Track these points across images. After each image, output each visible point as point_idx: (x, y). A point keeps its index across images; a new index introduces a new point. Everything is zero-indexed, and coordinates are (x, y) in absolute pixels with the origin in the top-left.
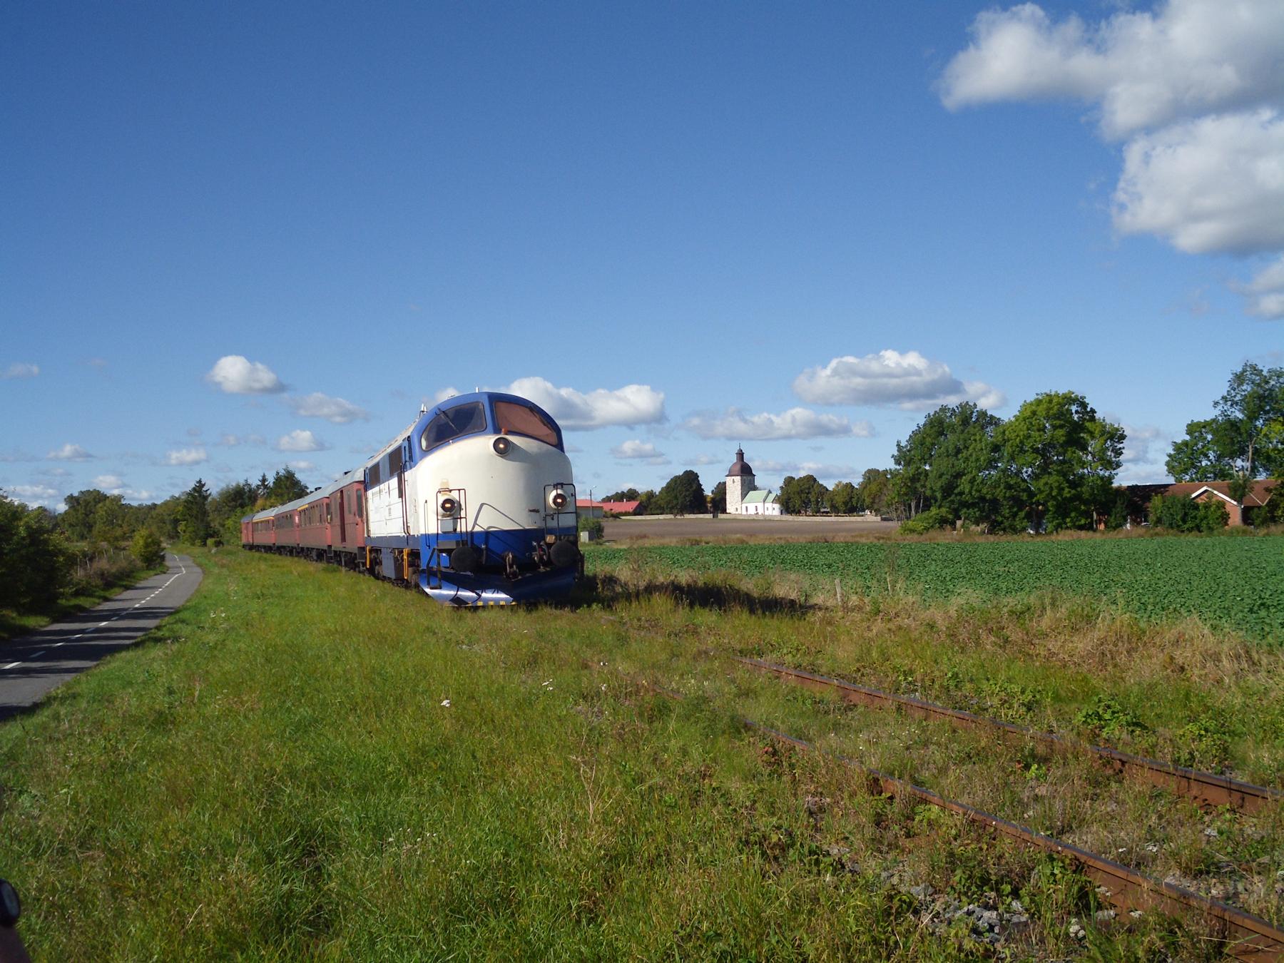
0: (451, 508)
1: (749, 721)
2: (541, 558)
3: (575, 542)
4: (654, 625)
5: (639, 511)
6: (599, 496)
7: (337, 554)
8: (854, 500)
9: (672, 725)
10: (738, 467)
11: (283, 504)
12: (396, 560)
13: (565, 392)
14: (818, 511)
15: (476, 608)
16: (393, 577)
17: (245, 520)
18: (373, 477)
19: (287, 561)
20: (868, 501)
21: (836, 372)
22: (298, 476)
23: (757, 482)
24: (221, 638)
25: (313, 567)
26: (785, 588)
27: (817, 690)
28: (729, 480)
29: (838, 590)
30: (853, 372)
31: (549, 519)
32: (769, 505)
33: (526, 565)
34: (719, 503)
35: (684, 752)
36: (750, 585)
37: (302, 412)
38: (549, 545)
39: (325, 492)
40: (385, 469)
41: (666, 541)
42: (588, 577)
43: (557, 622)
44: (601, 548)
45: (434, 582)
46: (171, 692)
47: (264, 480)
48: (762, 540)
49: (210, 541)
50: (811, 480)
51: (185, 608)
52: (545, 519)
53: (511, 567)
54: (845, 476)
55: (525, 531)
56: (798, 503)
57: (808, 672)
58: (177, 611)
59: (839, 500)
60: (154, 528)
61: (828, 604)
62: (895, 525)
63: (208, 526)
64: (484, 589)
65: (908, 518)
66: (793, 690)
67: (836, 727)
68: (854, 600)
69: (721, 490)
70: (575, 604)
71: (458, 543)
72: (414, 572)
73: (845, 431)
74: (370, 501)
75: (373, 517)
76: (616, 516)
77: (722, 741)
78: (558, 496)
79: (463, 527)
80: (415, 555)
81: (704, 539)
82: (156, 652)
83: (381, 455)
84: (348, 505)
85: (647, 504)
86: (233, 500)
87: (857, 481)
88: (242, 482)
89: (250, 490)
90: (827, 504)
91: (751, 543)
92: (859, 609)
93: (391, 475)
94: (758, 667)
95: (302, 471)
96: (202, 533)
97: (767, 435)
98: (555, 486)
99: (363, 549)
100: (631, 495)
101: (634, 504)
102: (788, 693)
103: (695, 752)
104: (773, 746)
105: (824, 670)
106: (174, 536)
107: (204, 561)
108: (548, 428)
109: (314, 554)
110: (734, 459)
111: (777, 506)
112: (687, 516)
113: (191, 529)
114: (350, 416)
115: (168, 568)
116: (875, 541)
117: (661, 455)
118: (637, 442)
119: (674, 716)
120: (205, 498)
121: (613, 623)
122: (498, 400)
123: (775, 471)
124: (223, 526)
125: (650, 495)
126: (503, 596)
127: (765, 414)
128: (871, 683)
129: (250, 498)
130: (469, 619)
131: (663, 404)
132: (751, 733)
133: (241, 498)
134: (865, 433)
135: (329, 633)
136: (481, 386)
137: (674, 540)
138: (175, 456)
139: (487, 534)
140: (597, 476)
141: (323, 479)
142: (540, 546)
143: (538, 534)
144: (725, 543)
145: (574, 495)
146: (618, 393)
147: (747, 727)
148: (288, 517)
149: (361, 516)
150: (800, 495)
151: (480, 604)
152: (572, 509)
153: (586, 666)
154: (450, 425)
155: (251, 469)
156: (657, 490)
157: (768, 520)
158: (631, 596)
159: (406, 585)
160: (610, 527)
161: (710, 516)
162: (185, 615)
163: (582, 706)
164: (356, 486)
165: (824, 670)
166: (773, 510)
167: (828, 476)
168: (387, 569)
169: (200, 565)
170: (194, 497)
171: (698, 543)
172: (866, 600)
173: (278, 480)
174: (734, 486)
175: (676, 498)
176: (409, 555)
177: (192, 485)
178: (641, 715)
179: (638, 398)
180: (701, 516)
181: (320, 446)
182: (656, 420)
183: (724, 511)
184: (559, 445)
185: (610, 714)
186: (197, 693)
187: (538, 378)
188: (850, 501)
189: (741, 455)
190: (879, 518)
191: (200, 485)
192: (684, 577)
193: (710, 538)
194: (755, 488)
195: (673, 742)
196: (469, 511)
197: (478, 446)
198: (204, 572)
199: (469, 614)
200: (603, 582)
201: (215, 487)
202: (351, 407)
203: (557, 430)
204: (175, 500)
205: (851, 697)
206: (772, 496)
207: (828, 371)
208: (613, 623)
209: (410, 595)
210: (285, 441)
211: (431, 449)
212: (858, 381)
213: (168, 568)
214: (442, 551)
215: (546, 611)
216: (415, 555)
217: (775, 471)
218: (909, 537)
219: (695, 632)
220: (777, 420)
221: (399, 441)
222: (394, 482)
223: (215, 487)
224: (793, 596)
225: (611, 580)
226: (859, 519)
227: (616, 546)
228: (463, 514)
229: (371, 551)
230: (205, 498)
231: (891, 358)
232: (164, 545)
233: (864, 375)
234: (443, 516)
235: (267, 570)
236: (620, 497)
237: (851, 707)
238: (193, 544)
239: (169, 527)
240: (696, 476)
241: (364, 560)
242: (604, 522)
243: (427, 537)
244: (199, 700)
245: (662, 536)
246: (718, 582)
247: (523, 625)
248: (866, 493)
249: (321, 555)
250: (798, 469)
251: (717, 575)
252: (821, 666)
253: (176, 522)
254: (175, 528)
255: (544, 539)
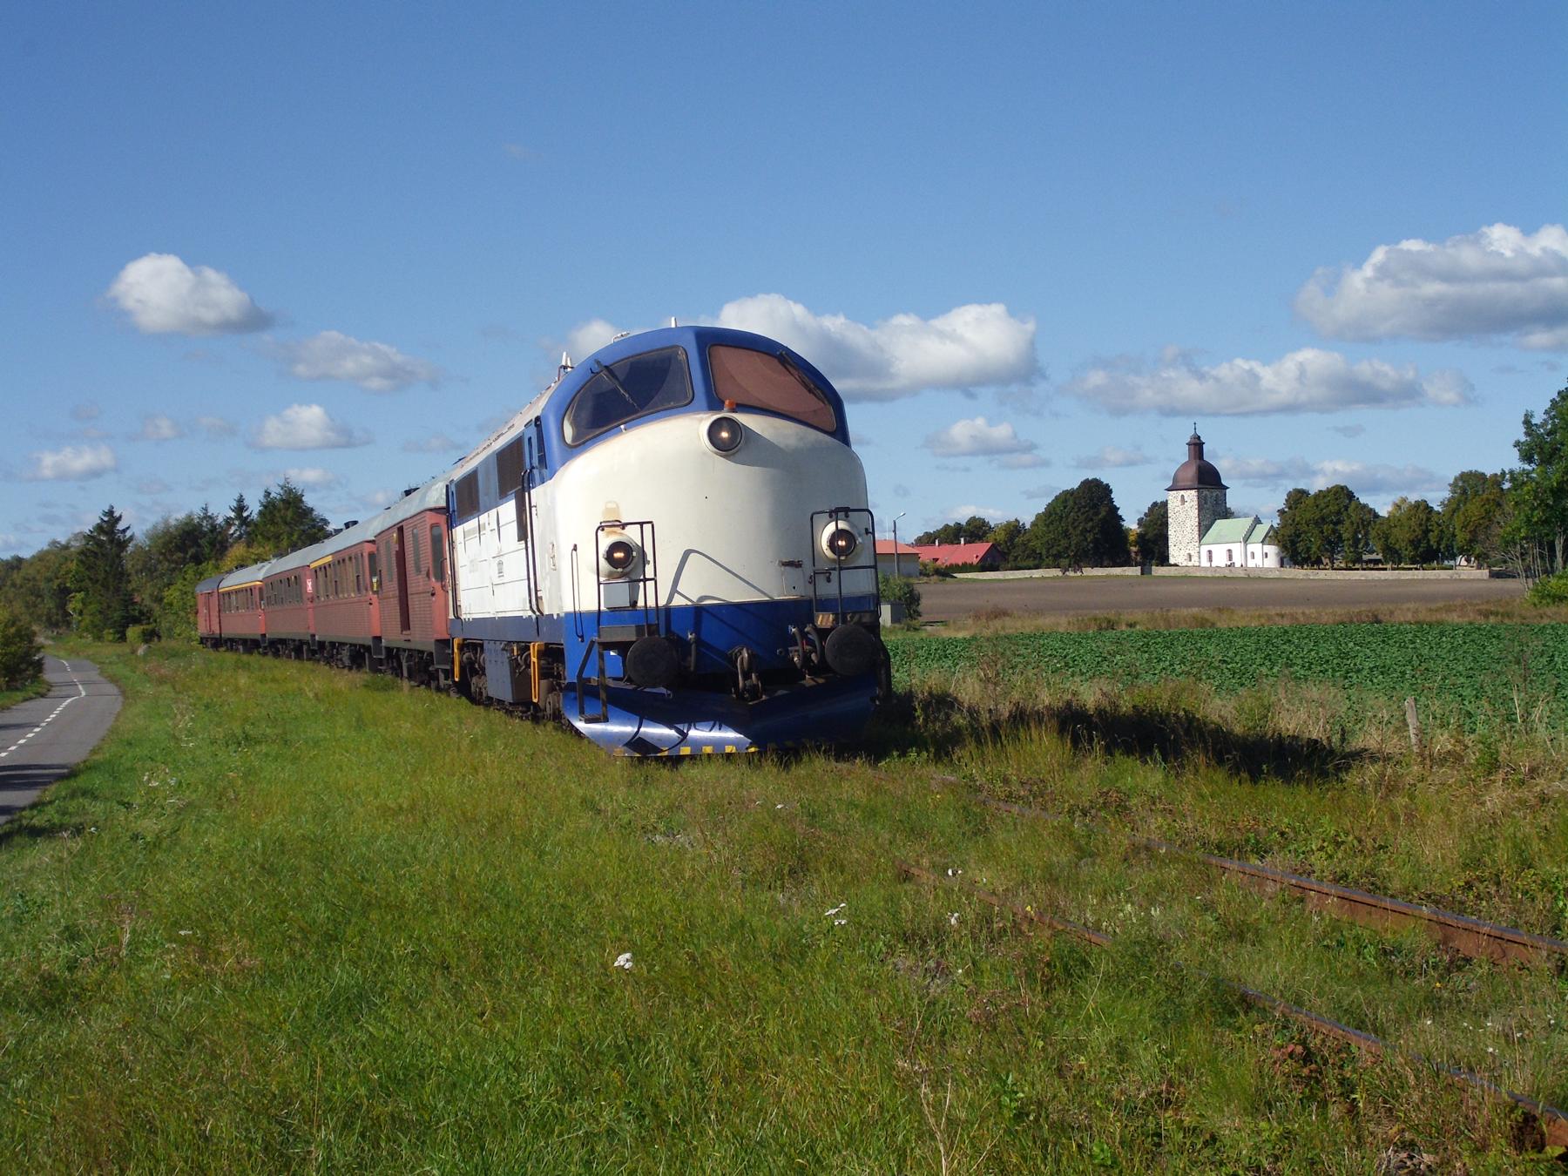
0: (625, 561)
1: (1252, 990)
2: (806, 658)
3: (875, 627)
4: (1039, 793)
5: (987, 564)
6: (910, 534)
7: (393, 654)
8: (1433, 537)
9: (1094, 997)
10: (1192, 472)
11: (281, 555)
12: (514, 665)
13: (835, 324)
14: (1358, 560)
15: (676, 761)
16: (508, 697)
17: (203, 588)
18: (465, 500)
19: (289, 669)
20: (1461, 537)
21: (1383, 272)
22: (309, 500)
23: (1232, 501)
24: (166, 824)
25: (345, 681)
26: (1300, 715)
27: (1391, 929)
28: (1173, 499)
29: (1411, 721)
30: (1422, 269)
31: (821, 580)
32: (1256, 548)
33: (775, 672)
34: (1153, 544)
35: (1122, 1053)
36: (1221, 708)
37: (301, 369)
38: (823, 633)
39: (370, 528)
40: (488, 484)
41: (1045, 622)
42: (898, 697)
43: (839, 785)
44: (917, 636)
45: (593, 708)
46: (72, 934)
47: (240, 508)
48: (1243, 619)
49: (133, 632)
50: (1342, 496)
51: (89, 767)
52: (812, 580)
53: (747, 676)
54: (1411, 486)
55: (772, 606)
56: (1315, 544)
57: (1366, 891)
58: (72, 773)
59: (1401, 537)
60: (18, 607)
61: (1389, 748)
62: (1520, 587)
63: (128, 601)
64: (693, 721)
65: (1549, 572)
66: (1335, 926)
67: (1434, 1005)
68: (1443, 742)
69: (1158, 518)
70: (876, 751)
71: (639, 630)
72: (551, 689)
73: (1408, 393)
74: (459, 548)
75: (465, 579)
76: (945, 573)
77: (1197, 1035)
78: (838, 534)
79: (652, 596)
80: (553, 654)
81: (1127, 617)
82: (41, 854)
83: (480, 454)
84: (415, 556)
85: (1008, 548)
86: (182, 548)
87: (1437, 497)
88: (197, 512)
89: (213, 528)
90: (1376, 544)
91: (1222, 625)
92: (1456, 758)
93: (503, 495)
94: (1259, 878)
95: (314, 487)
96: (116, 615)
97: (1247, 406)
98: (834, 514)
99: (445, 643)
100: (975, 530)
101: (981, 548)
102: (1326, 935)
103: (1146, 1055)
104: (1303, 1043)
105: (1395, 885)
106: (60, 621)
107: (120, 670)
108: (813, 395)
109: (345, 654)
110: (1182, 455)
111: (1272, 550)
112: (1088, 572)
113: (93, 607)
114: (398, 377)
115: (50, 686)
116: (1480, 620)
117: (1030, 448)
118: (980, 421)
119: (1096, 980)
120: (122, 545)
121: (953, 788)
122: (712, 341)
123: (1266, 478)
124: (159, 600)
125: (1014, 529)
126: (731, 734)
127: (1239, 362)
128: (1497, 913)
129: (212, 544)
130: (667, 785)
131: (1032, 344)
132: (1254, 1015)
133: (196, 545)
134: (1449, 396)
135: (386, 812)
136: (673, 317)
137: (1063, 620)
138: (49, 459)
139: (698, 613)
140: (910, 496)
141: (361, 501)
142: (804, 635)
143: (800, 611)
144: (1169, 626)
145: (870, 532)
146: (938, 323)
147: (1247, 1003)
148: (291, 581)
149: (441, 576)
150: (1321, 527)
151: (685, 751)
152: (865, 559)
153: (906, 876)
154: (619, 393)
155: (214, 489)
156: (1027, 519)
157: (1253, 577)
158: (999, 731)
159: (535, 715)
160: (932, 595)
161: (1136, 571)
162: (97, 781)
163: (904, 960)
164: (431, 519)
165: (1395, 885)
166: (1263, 557)
167: (1376, 487)
168: (497, 681)
169: (114, 680)
170: (100, 544)
171: (1111, 625)
172: (1469, 739)
173: (269, 507)
174: (1184, 510)
175: (1066, 534)
176: (541, 655)
177: (90, 520)
178: (1029, 975)
179: (979, 333)
180: (1117, 571)
181: (344, 438)
182: (1018, 378)
183: (1164, 560)
184: (840, 432)
185: (967, 974)
186: (126, 938)
187: (774, 297)
188: (1424, 538)
189: (1197, 446)
190: (1485, 573)
191: (112, 519)
192: (1090, 695)
193: (1139, 615)
194: (1227, 514)
195: (1097, 1031)
196: (663, 566)
197: (673, 441)
198: (123, 693)
199: (665, 772)
200: (926, 706)
201: (140, 524)
202: (399, 359)
203: (834, 402)
204: (59, 551)
205: (1455, 944)
206: (1262, 530)
207: (1368, 271)
208: (953, 788)
209: (546, 734)
210: (273, 431)
211: (582, 442)
212: (1432, 288)
213: (50, 686)
214: (608, 646)
215: (818, 766)
216: (553, 654)
217: (1266, 478)
218: (1553, 609)
219: (1122, 809)
220: (1267, 375)
221: (517, 427)
222: (509, 509)
223: (140, 524)
224: (1316, 733)
225: (942, 702)
226: (1444, 574)
227: (946, 633)
228: (649, 573)
229: (462, 648)
230: (122, 545)
231: (1503, 239)
232: (40, 640)
233: (1448, 277)
234: (610, 575)
235: (248, 685)
236: (952, 534)
237: (1461, 963)
238: (99, 638)
239: (49, 604)
240: (1107, 490)
241: (450, 665)
242: (922, 586)
243: (577, 618)
244: (132, 953)
245: (1039, 612)
246: (1162, 705)
247: (774, 790)
248: (1458, 522)
249: (360, 656)
250: (1314, 473)
251: (1156, 690)
252: (1389, 877)
253: (63, 593)
254: (62, 606)
255: (812, 620)
